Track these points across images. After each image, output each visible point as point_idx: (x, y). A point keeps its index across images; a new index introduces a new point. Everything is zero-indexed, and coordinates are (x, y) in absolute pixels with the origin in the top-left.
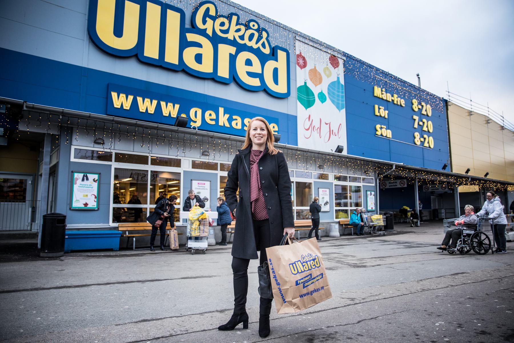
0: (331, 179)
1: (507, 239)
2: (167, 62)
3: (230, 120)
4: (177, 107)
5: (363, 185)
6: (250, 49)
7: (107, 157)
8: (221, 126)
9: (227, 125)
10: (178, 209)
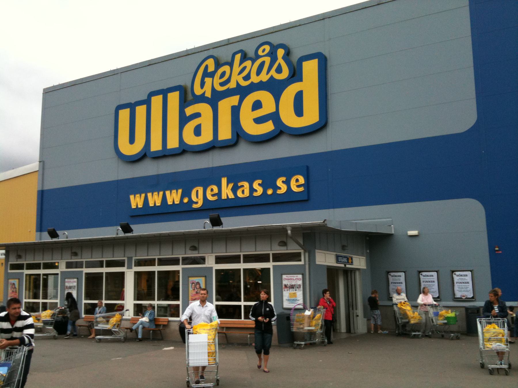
0: (211, 263)
3: (234, 190)
5: (183, 269)
7: (20, 267)
9: (231, 196)
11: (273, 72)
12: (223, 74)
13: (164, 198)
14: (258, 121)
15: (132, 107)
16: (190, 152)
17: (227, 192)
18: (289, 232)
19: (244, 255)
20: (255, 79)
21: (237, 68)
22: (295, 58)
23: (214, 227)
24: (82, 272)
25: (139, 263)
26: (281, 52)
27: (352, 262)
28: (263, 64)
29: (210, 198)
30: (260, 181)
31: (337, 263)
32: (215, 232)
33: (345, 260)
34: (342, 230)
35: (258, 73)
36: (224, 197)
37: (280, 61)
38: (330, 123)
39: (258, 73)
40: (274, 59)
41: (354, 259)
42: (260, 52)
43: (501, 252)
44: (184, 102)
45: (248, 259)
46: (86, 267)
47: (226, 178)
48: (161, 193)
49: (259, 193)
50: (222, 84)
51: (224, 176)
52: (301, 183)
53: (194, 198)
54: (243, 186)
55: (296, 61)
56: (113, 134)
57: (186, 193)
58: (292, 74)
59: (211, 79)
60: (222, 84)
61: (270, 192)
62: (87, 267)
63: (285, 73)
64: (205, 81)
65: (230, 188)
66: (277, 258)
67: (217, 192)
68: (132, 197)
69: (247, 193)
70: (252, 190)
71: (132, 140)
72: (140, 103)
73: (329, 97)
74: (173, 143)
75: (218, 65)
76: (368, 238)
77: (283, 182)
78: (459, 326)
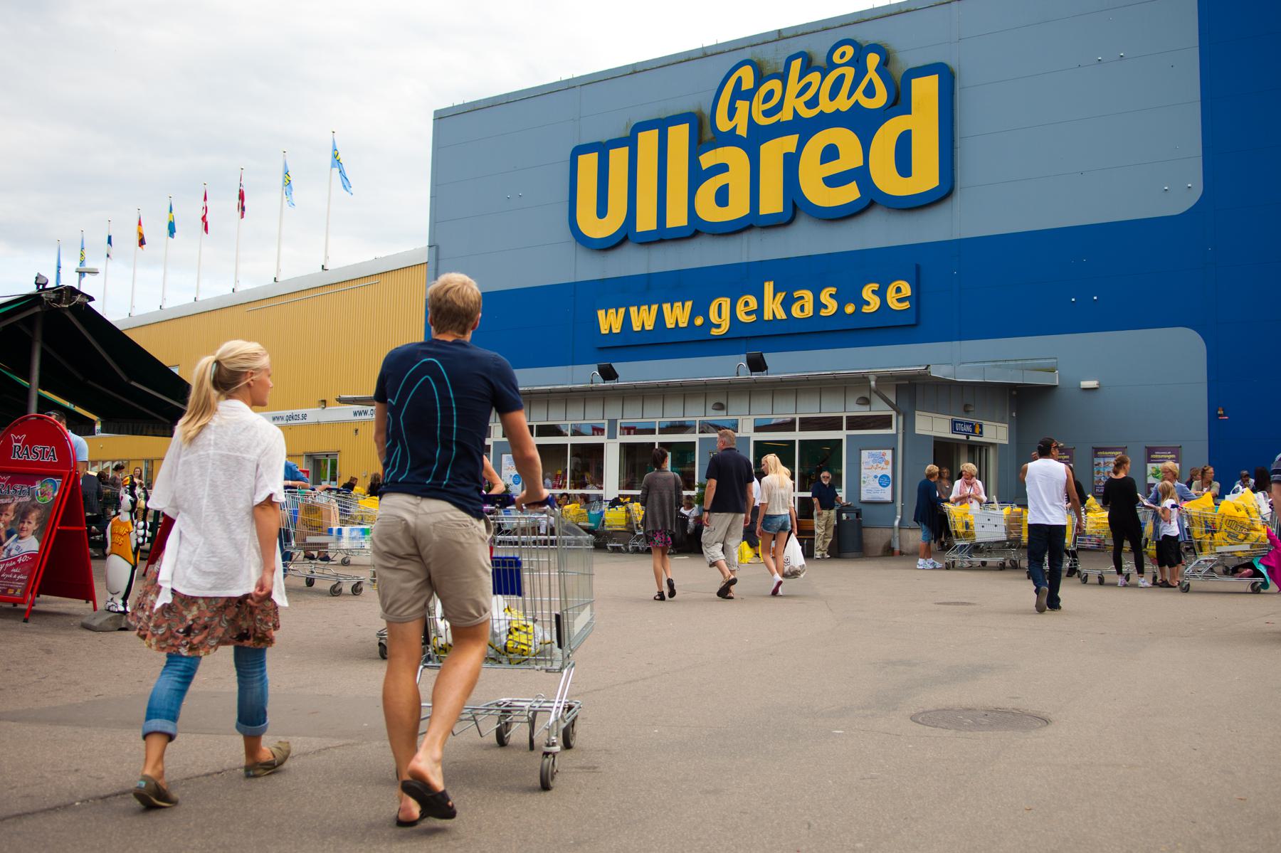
1: (1026, 550)
3: (787, 305)
5: (701, 439)
9: (781, 315)
11: (859, 95)
12: (770, 95)
14: (832, 181)
15: (603, 149)
17: (773, 307)
18: (873, 383)
20: (826, 106)
21: (794, 85)
22: (899, 68)
23: (753, 373)
25: (629, 430)
26: (873, 60)
27: (981, 432)
29: (742, 317)
30: (833, 290)
31: (953, 433)
32: (755, 382)
33: (969, 428)
35: (833, 95)
36: (768, 316)
37: (872, 74)
39: (833, 95)
40: (861, 72)
41: (985, 428)
42: (836, 58)
43: (1226, 418)
44: (699, 144)
45: (807, 424)
47: (766, 318)
48: (655, 308)
50: (767, 114)
53: (714, 317)
54: (802, 298)
55: (901, 76)
57: (701, 309)
58: (893, 98)
59: (748, 102)
60: (767, 114)
66: (855, 423)
68: (601, 313)
70: (818, 305)
71: (602, 211)
73: (958, 143)
74: (677, 218)
75: (760, 78)
78: (1201, 551)
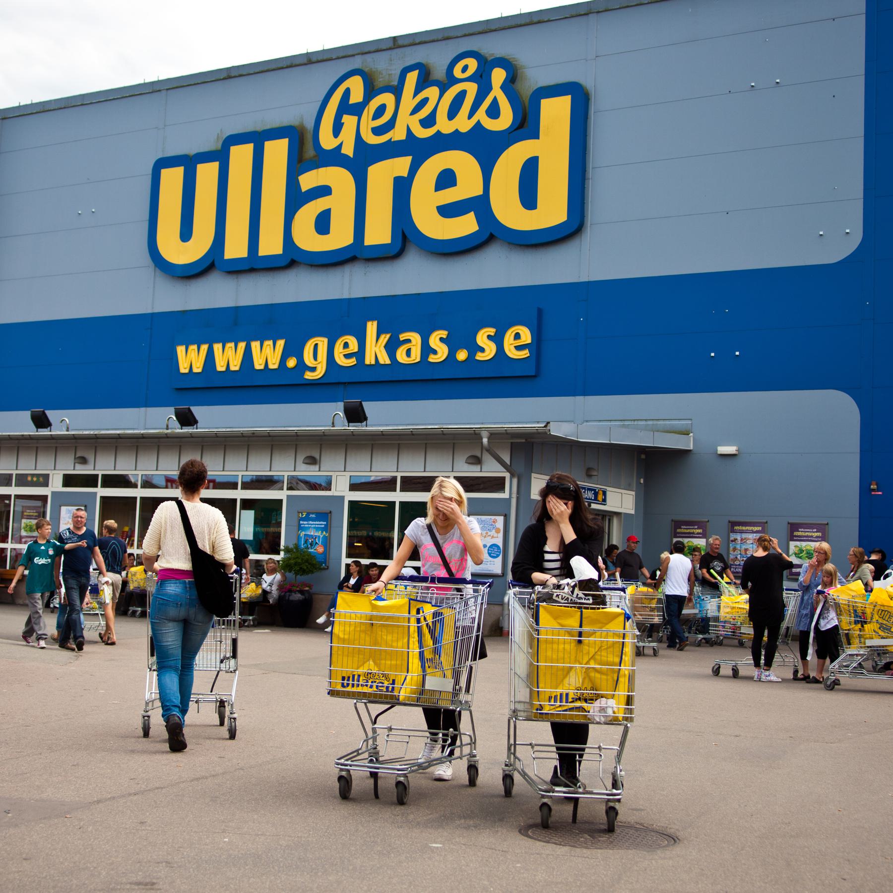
2: (261, 256)
3: (391, 348)
4: (181, 351)
6: (442, 143)
7: (90, 481)
8: (370, 365)
9: (384, 359)
10: (472, 575)
11: (481, 115)
13: (248, 355)
14: (448, 211)
16: (305, 264)
19: (402, 477)
20: (444, 125)
21: (408, 100)
24: (95, 493)
26: (498, 76)
27: (604, 500)
28: (460, 97)
29: (341, 360)
30: (444, 334)
32: (353, 434)
34: (579, 440)
35: (452, 113)
36: (369, 360)
37: (497, 92)
38: (589, 225)
39: (452, 113)
40: (484, 89)
41: (608, 494)
42: (457, 72)
43: (880, 493)
46: (103, 486)
49: (442, 355)
50: (377, 131)
51: (372, 320)
52: (524, 341)
54: (409, 341)
56: (147, 217)
57: (294, 349)
59: (356, 118)
60: (377, 131)
61: (462, 355)
62: (105, 485)
63: (505, 120)
64: (342, 121)
65: (382, 343)
67: (356, 350)
68: (181, 350)
69: (416, 356)
70: (427, 350)
71: (186, 233)
72: (206, 157)
73: (590, 173)
75: (371, 91)
76: (643, 456)
77: (489, 337)
